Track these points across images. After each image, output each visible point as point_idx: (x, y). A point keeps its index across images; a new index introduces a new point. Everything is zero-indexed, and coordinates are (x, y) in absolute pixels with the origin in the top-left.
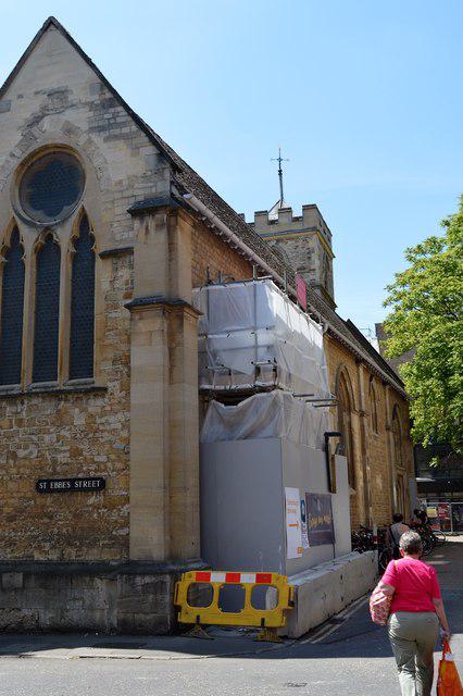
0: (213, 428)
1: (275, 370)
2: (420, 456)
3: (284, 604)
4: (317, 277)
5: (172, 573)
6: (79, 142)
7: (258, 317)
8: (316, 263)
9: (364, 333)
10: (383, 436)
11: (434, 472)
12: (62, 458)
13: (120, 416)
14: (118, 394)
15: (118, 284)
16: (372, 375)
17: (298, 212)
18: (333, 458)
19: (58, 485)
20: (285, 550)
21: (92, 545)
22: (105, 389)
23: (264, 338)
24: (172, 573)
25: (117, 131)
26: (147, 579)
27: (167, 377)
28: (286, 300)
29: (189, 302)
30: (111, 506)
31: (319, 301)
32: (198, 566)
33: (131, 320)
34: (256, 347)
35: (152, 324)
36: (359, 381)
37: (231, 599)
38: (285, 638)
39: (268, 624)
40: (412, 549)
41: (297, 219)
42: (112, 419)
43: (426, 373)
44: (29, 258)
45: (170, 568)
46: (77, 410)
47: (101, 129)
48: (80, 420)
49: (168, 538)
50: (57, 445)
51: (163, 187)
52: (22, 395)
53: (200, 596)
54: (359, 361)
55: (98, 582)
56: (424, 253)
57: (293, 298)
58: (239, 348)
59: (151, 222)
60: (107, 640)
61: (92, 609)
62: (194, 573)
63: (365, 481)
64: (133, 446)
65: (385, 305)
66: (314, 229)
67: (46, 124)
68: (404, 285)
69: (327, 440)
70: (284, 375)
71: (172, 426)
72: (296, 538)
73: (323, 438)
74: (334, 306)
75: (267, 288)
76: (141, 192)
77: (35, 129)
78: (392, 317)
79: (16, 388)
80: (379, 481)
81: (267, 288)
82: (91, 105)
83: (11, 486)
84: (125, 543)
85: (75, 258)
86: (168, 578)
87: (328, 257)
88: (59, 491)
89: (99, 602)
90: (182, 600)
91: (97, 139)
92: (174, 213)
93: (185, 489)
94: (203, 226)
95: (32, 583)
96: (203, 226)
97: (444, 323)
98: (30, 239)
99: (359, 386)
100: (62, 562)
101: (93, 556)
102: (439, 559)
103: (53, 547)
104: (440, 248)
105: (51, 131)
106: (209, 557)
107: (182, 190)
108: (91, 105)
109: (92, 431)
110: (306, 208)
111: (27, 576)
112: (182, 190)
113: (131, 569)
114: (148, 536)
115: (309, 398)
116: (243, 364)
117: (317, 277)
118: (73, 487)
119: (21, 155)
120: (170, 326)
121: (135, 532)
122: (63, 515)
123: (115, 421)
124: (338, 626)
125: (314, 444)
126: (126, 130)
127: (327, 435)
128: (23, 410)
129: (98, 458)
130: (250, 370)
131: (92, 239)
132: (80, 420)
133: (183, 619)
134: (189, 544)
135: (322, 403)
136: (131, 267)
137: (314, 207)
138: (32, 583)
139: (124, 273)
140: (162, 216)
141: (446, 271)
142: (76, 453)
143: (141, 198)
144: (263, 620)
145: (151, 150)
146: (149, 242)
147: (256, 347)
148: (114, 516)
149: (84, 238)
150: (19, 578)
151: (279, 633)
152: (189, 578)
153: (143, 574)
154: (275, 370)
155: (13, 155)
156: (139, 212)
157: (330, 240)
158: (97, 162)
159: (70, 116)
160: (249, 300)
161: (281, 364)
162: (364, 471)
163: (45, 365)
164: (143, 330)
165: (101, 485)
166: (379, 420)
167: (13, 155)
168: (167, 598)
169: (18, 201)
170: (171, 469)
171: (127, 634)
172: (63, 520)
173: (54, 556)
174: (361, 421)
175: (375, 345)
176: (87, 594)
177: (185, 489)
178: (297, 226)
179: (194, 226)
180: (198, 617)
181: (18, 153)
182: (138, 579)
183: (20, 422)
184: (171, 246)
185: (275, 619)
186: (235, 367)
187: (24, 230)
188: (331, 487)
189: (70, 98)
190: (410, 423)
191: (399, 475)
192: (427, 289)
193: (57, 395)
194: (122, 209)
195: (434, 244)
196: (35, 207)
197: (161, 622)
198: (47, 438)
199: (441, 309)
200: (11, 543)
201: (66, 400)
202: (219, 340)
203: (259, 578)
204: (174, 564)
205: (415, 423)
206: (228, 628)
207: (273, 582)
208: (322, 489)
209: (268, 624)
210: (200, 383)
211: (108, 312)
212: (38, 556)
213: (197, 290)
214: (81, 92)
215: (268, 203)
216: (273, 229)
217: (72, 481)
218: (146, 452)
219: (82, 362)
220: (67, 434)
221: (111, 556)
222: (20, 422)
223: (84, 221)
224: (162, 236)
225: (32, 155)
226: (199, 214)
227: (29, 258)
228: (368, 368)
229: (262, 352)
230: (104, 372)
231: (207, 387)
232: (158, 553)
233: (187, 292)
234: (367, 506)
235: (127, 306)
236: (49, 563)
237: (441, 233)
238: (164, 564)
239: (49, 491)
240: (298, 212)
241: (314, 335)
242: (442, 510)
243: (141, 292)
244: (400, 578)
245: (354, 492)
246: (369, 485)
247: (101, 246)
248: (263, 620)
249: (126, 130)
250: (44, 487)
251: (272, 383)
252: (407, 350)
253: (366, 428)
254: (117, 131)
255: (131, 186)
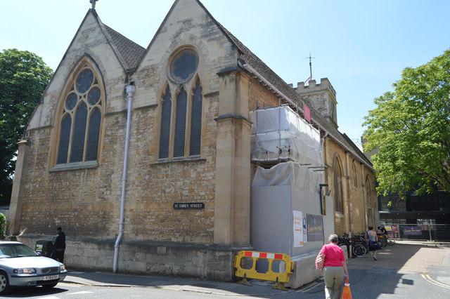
0: (258, 179)
1: (289, 151)
2: (381, 202)
3: (288, 271)
4: (328, 112)
5: (233, 251)
6: (196, 43)
7: (281, 125)
8: (327, 106)
9: (354, 141)
10: (360, 189)
11: (390, 208)
12: (185, 193)
13: (212, 173)
14: (211, 163)
15: (212, 109)
16: (354, 159)
17: (318, 82)
18: (324, 198)
19: (183, 206)
20: (292, 242)
21: (197, 235)
22: (205, 160)
23: (284, 135)
24: (233, 251)
25: (213, 37)
26: (222, 254)
27: (234, 154)
28: (297, 117)
29: (247, 117)
30: (206, 217)
31: (326, 122)
32: (248, 248)
33: (217, 126)
34: (280, 139)
35: (227, 128)
36: (346, 162)
37: (261, 266)
38: (289, 288)
39: (279, 280)
40: (333, 241)
41: (318, 85)
42: (208, 174)
43: (383, 159)
44: (173, 99)
45: (232, 249)
46: (192, 170)
47: (206, 36)
48: (193, 175)
49: (232, 234)
50: (183, 187)
51: (234, 62)
52: (168, 163)
53: (246, 264)
54: (346, 152)
55: (200, 254)
56: (383, 100)
57: (303, 117)
58: (272, 141)
59: (227, 78)
60: (203, 283)
61: (196, 266)
62: (244, 252)
63: (349, 211)
64: (217, 188)
65: (363, 125)
66: (326, 89)
67: (182, 36)
68: (373, 116)
69: (321, 188)
70: (294, 154)
71: (235, 179)
72: (299, 237)
73: (319, 187)
74: (337, 127)
75: (286, 110)
76: (224, 65)
77: (177, 39)
78: (366, 131)
79: (166, 160)
80: (357, 211)
81: (286, 110)
82: (202, 25)
83: (163, 205)
84: (211, 235)
85: (193, 98)
86: (231, 253)
87: (334, 104)
88: (183, 208)
89: (199, 263)
90: (238, 265)
91: (204, 41)
92: (238, 74)
93: (242, 209)
94: (255, 80)
95: (170, 252)
96: (255, 80)
97: (394, 134)
98: (174, 89)
99: (347, 167)
100: (184, 243)
101: (197, 240)
102: (388, 252)
103: (180, 235)
104: (392, 98)
105: (184, 39)
106: (253, 244)
107: (243, 62)
108: (202, 25)
109: (199, 180)
110: (322, 80)
111: (168, 248)
112: (243, 62)
113: (214, 248)
114: (222, 233)
115: (309, 166)
116: (273, 148)
117: (328, 112)
118: (190, 207)
119: (171, 51)
120: (236, 129)
121: (216, 230)
122: (185, 219)
123: (209, 175)
124: (319, 284)
125: (313, 190)
126: (217, 36)
127: (321, 186)
128: (168, 170)
129: (201, 194)
130: (277, 151)
131: (201, 88)
132: (193, 175)
133: (238, 274)
134: (244, 237)
135: (319, 169)
136: (218, 101)
137: (326, 79)
138: (170, 252)
139: (215, 104)
140: (233, 75)
141: (395, 108)
142: (191, 191)
143: (224, 67)
144: (277, 278)
145: (228, 44)
146: (226, 89)
147: (280, 139)
148: (208, 222)
149: (198, 88)
150: (164, 250)
151: (286, 285)
152: (241, 255)
153: (219, 251)
154: (289, 151)
155: (167, 52)
156: (221, 74)
157: (335, 95)
158: (204, 52)
159: (193, 31)
160: (277, 117)
161: (293, 148)
162: (349, 206)
163: (179, 151)
164: (223, 131)
165: (202, 206)
166: (358, 182)
167: (167, 52)
168: (231, 264)
169: (169, 73)
170: (234, 199)
171: (210, 281)
172: (185, 223)
173: (180, 240)
174: (348, 181)
175: (361, 149)
176: (194, 259)
177: (242, 209)
178: (318, 88)
179: (250, 80)
180: (245, 274)
181: (170, 50)
182: (217, 253)
183: (167, 176)
184: (237, 90)
185: (283, 278)
186: (270, 149)
187: (171, 86)
188: (323, 212)
189: (193, 22)
190: (377, 184)
191: (369, 209)
192: (384, 117)
193: (184, 163)
194: (214, 74)
195: (389, 95)
196: (177, 75)
197: (227, 276)
198: (179, 183)
199: (392, 127)
200: (162, 233)
201: (188, 165)
202: (262, 136)
203: (276, 256)
204: (235, 246)
205: (380, 184)
206: (262, 281)
207: (283, 259)
208: (318, 213)
209: (279, 280)
210: (251, 158)
211: (207, 124)
212: (174, 240)
213: (252, 112)
214: (198, 20)
215: (304, 78)
216: (306, 90)
217: (189, 204)
218: (223, 190)
219: (195, 149)
220: (187, 181)
221: (205, 241)
222: (167, 176)
223: (198, 80)
224: (232, 86)
225: (176, 50)
226: (252, 75)
227: (173, 99)
228: (352, 155)
229: (283, 142)
230: (205, 152)
231: (255, 159)
232: (227, 241)
233: (244, 112)
234: (350, 223)
235: (216, 120)
236: (178, 243)
237: (392, 90)
238: (230, 246)
239: (179, 208)
240: (318, 82)
241: (315, 135)
242: (394, 228)
243: (222, 113)
244: (327, 252)
245: (343, 216)
246: (351, 213)
247: (205, 91)
248: (277, 278)
249: (217, 36)
250: (177, 206)
251: (287, 157)
252: (375, 148)
253: (350, 185)
254: (213, 37)
255: (219, 62)
